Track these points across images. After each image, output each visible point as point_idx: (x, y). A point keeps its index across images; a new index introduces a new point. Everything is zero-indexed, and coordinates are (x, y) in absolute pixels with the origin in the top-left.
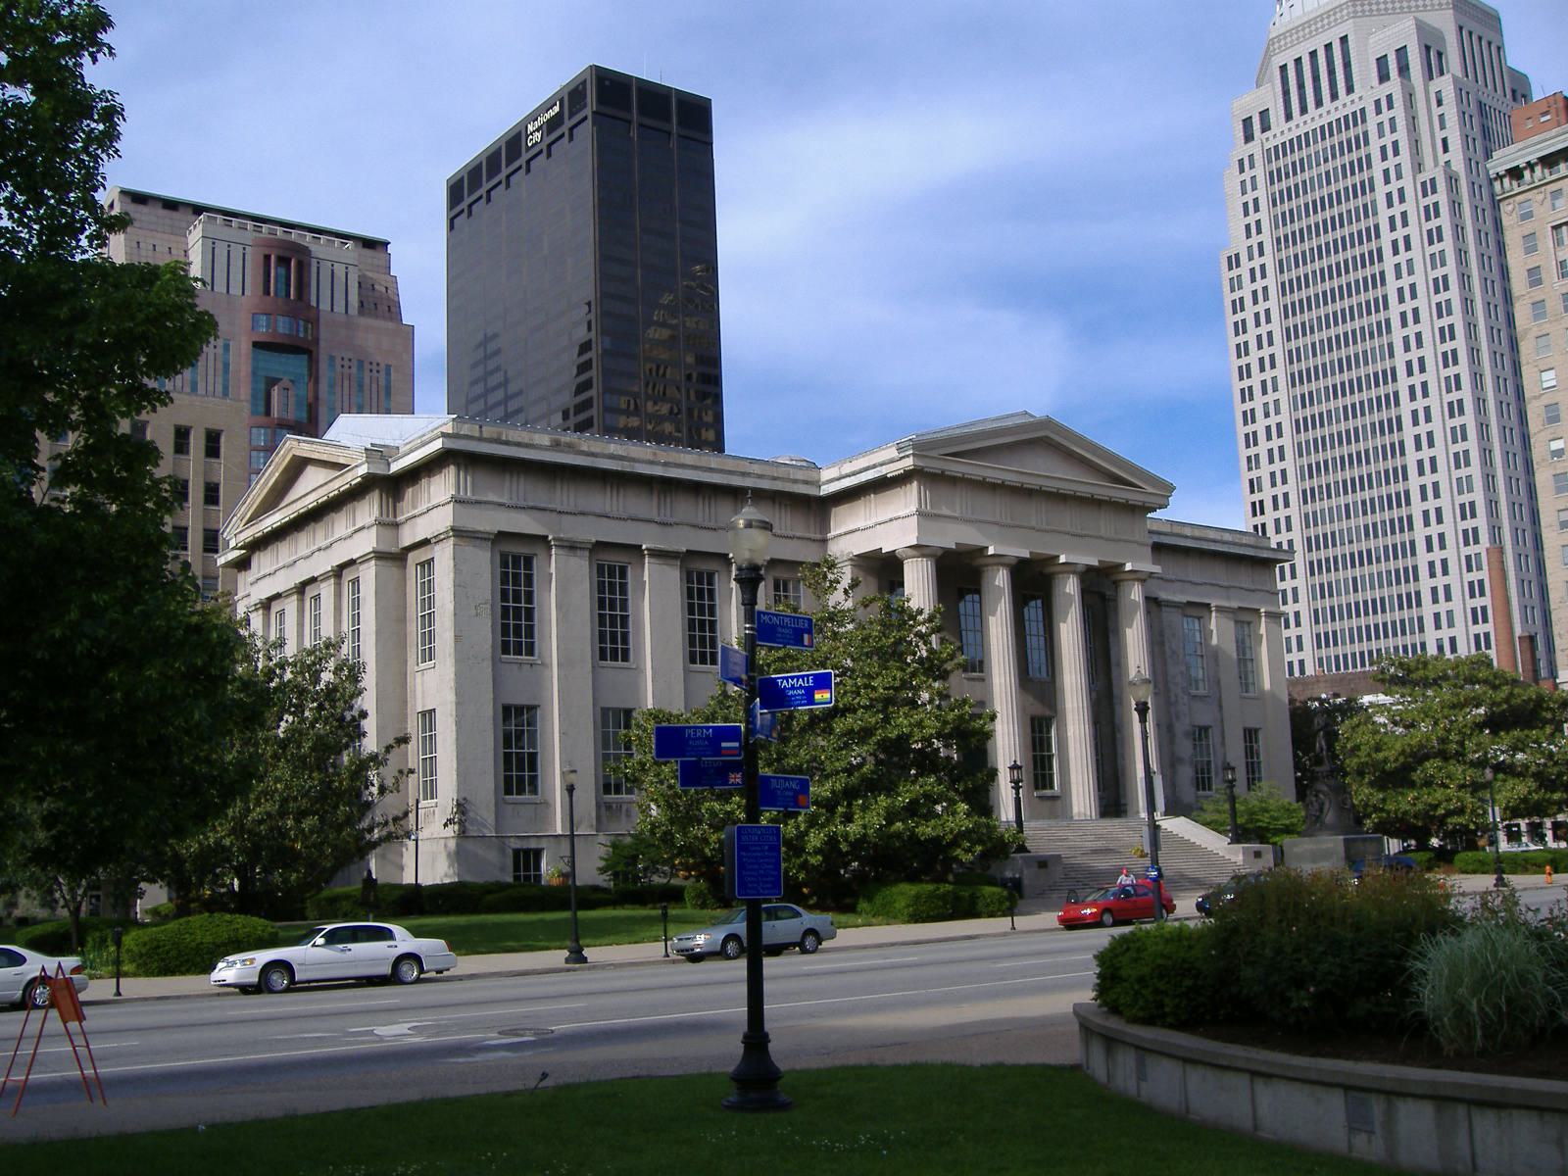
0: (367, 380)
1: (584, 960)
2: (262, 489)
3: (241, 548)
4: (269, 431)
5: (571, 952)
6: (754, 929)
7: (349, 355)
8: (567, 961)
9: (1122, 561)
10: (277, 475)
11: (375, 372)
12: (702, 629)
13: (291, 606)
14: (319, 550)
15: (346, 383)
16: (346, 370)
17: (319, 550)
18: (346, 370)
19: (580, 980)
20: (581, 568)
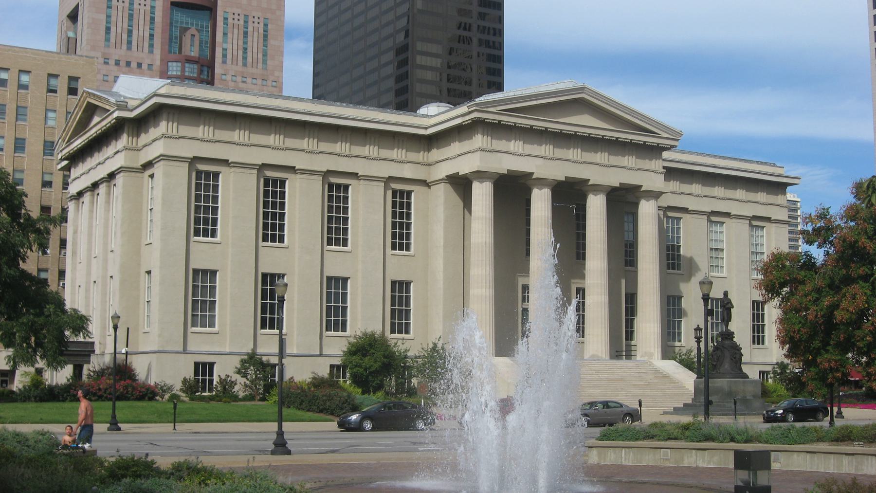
0: (250, 29)
1: (119, 429)
2: (73, 122)
3: (65, 159)
4: (179, 64)
5: (110, 424)
6: (626, 231)
7: (237, 11)
8: (109, 429)
9: (697, 380)
10: (80, 113)
11: (256, 23)
12: (401, 228)
13: (102, 189)
14: (99, 164)
15: (236, 31)
16: (236, 21)
17: (99, 164)
18: (236, 21)
19: (115, 436)
20: (316, 186)
